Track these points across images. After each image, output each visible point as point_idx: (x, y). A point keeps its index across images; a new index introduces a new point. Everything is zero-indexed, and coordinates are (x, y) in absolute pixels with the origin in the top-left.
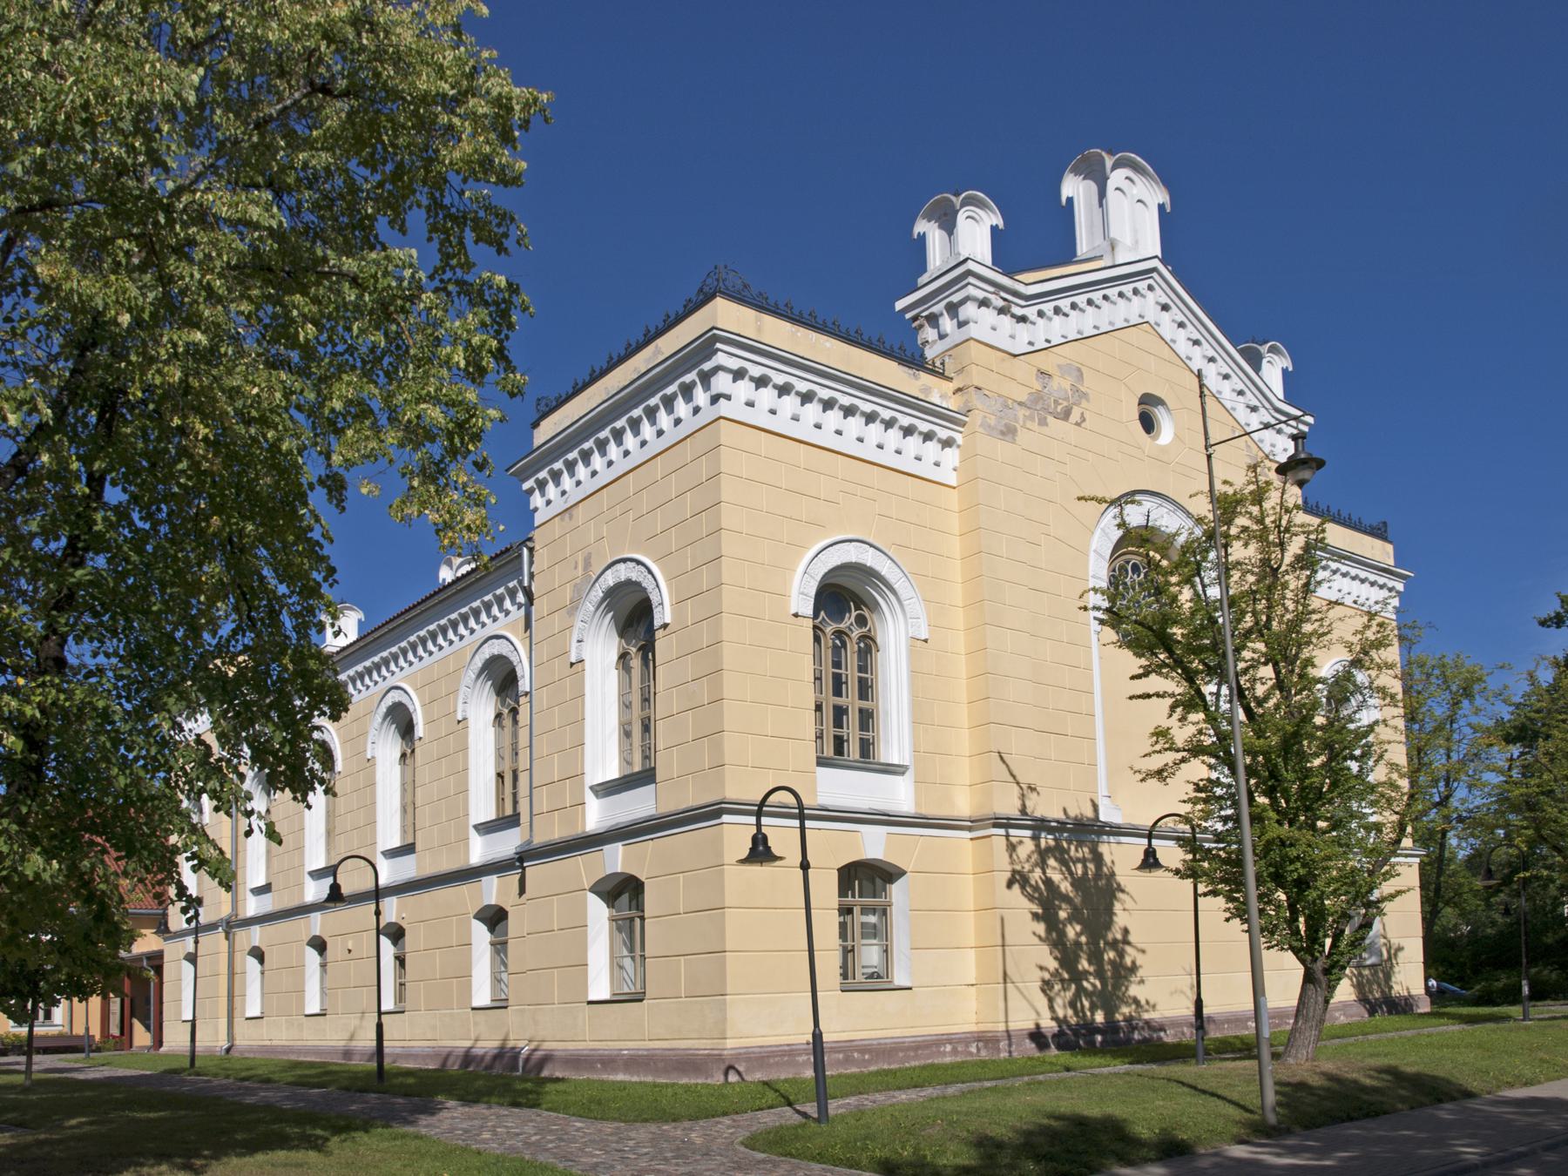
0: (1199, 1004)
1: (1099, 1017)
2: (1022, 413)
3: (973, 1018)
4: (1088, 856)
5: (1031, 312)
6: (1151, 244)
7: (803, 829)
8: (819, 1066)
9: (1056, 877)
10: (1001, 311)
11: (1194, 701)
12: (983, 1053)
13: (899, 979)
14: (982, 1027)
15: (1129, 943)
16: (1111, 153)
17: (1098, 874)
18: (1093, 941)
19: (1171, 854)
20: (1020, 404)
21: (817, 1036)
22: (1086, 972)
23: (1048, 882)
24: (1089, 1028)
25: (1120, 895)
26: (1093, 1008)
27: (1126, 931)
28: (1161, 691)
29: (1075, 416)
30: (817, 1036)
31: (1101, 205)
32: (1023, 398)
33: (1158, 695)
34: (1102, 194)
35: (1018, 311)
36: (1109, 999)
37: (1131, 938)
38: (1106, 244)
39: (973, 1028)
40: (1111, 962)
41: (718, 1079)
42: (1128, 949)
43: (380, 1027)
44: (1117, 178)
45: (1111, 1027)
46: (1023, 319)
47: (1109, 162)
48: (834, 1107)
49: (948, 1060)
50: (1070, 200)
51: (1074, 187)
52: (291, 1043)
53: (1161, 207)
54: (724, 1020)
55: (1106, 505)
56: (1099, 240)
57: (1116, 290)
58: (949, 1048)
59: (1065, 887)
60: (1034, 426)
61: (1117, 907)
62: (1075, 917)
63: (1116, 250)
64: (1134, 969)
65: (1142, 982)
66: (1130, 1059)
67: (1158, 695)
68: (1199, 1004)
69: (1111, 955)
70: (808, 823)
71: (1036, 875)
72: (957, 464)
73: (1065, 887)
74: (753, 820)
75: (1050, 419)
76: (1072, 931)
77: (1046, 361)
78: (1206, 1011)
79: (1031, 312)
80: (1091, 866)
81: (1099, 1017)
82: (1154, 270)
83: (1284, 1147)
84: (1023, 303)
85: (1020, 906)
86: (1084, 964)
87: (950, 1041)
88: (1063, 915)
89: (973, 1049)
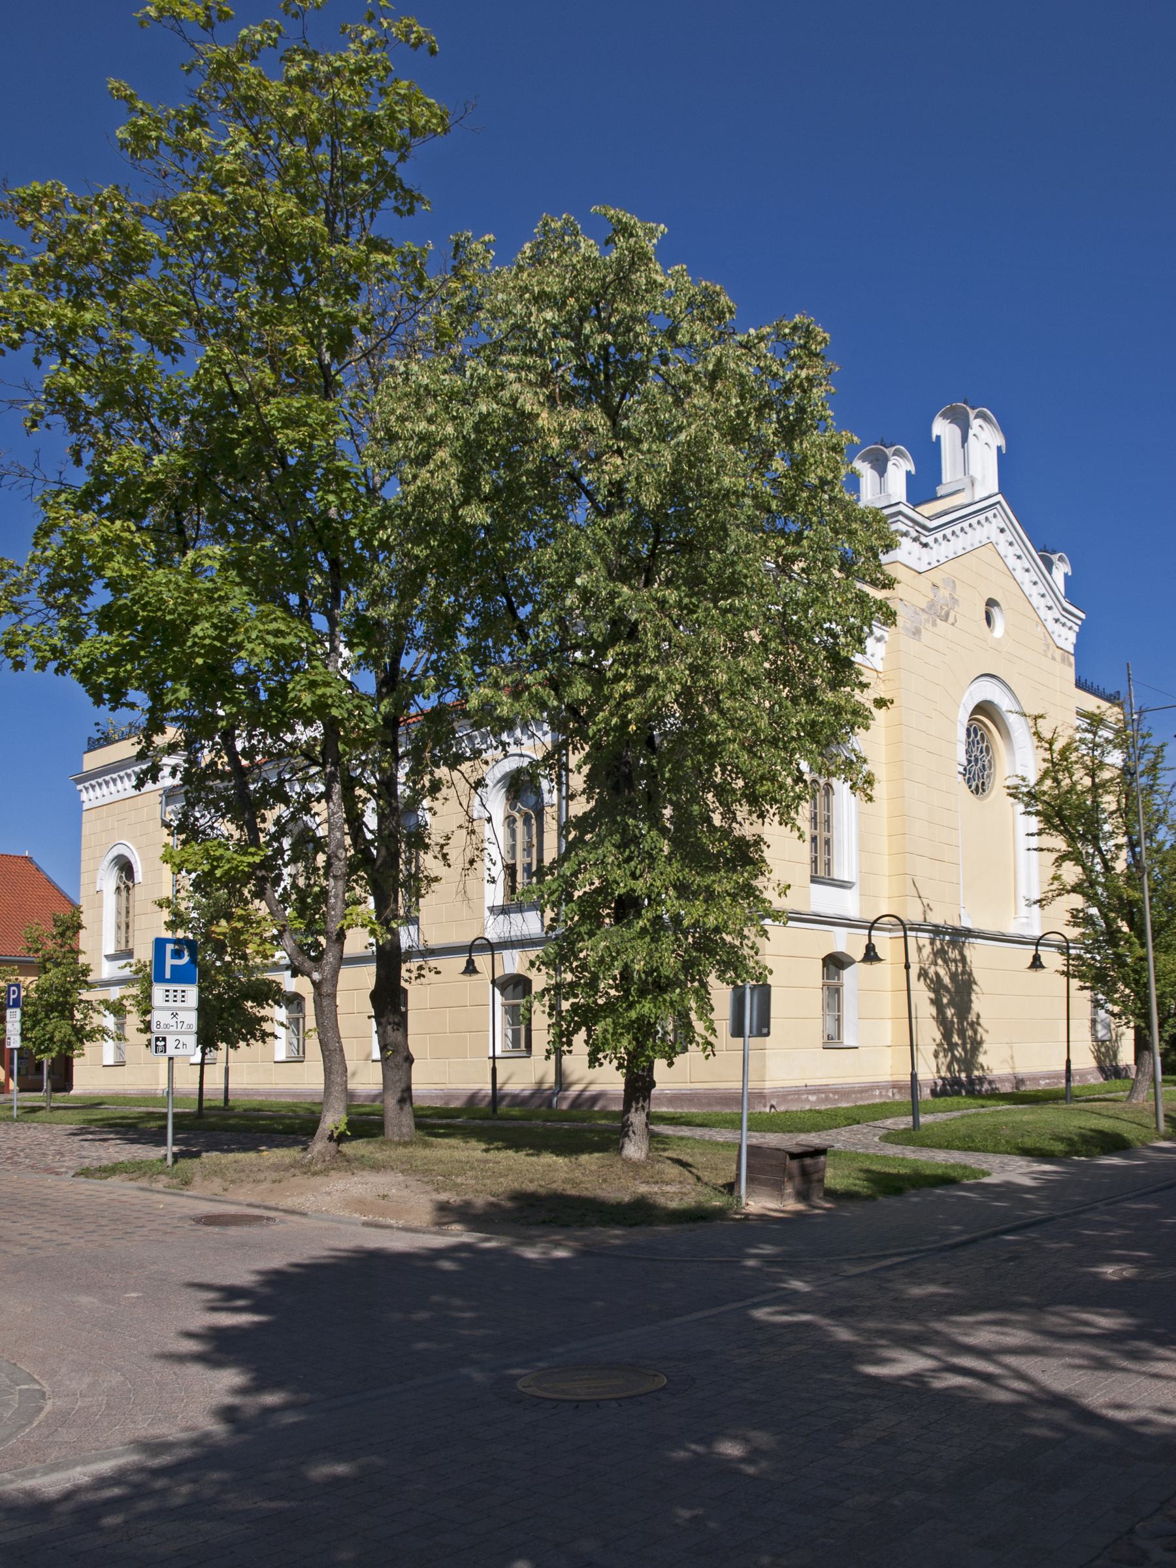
0: (1068, 1061)
1: (963, 1075)
2: (924, 616)
3: (889, 1071)
4: (958, 957)
5: (929, 540)
6: (992, 485)
7: (905, 937)
8: (1068, 1080)
9: (942, 972)
10: (915, 540)
11: (1075, 857)
12: (897, 1097)
13: (847, 1040)
14: (895, 1078)
15: (979, 1024)
16: (973, 408)
17: (964, 972)
18: (960, 1023)
19: (1053, 960)
20: (923, 610)
21: (914, 1076)
22: (957, 1044)
23: (937, 974)
24: (956, 1081)
25: (974, 987)
26: (959, 1071)
27: (978, 1016)
28: (1051, 846)
29: (951, 620)
30: (914, 1076)
31: (963, 447)
32: (924, 606)
33: (1048, 850)
34: (965, 439)
35: (924, 540)
36: (969, 1063)
37: (981, 1021)
38: (967, 481)
39: (889, 1078)
40: (970, 1037)
41: (767, 1110)
42: (980, 1029)
43: (494, 1070)
44: (976, 423)
45: (971, 1081)
46: (925, 545)
47: (972, 414)
48: (924, 1119)
49: (877, 1101)
50: (938, 437)
51: (942, 428)
52: (249, 1087)
53: (999, 449)
54: (764, 1067)
55: (1018, 709)
56: (960, 475)
57: (976, 520)
58: (877, 1092)
59: (947, 980)
60: (929, 626)
61: (973, 997)
62: (951, 1003)
63: (976, 485)
64: (980, 1043)
65: (985, 1053)
66: (500, 1144)
67: (1048, 850)
68: (1068, 1061)
69: (970, 1033)
70: (909, 933)
71: (931, 971)
72: (883, 655)
73: (947, 980)
74: (866, 932)
75: (938, 621)
76: (950, 1012)
77: (936, 576)
78: (1073, 1067)
79: (929, 540)
80: (960, 965)
81: (963, 1075)
82: (999, 503)
83: (550, 1242)
84: (927, 533)
85: (922, 994)
86: (956, 1039)
87: (878, 1087)
88: (945, 1001)
89: (890, 1094)
